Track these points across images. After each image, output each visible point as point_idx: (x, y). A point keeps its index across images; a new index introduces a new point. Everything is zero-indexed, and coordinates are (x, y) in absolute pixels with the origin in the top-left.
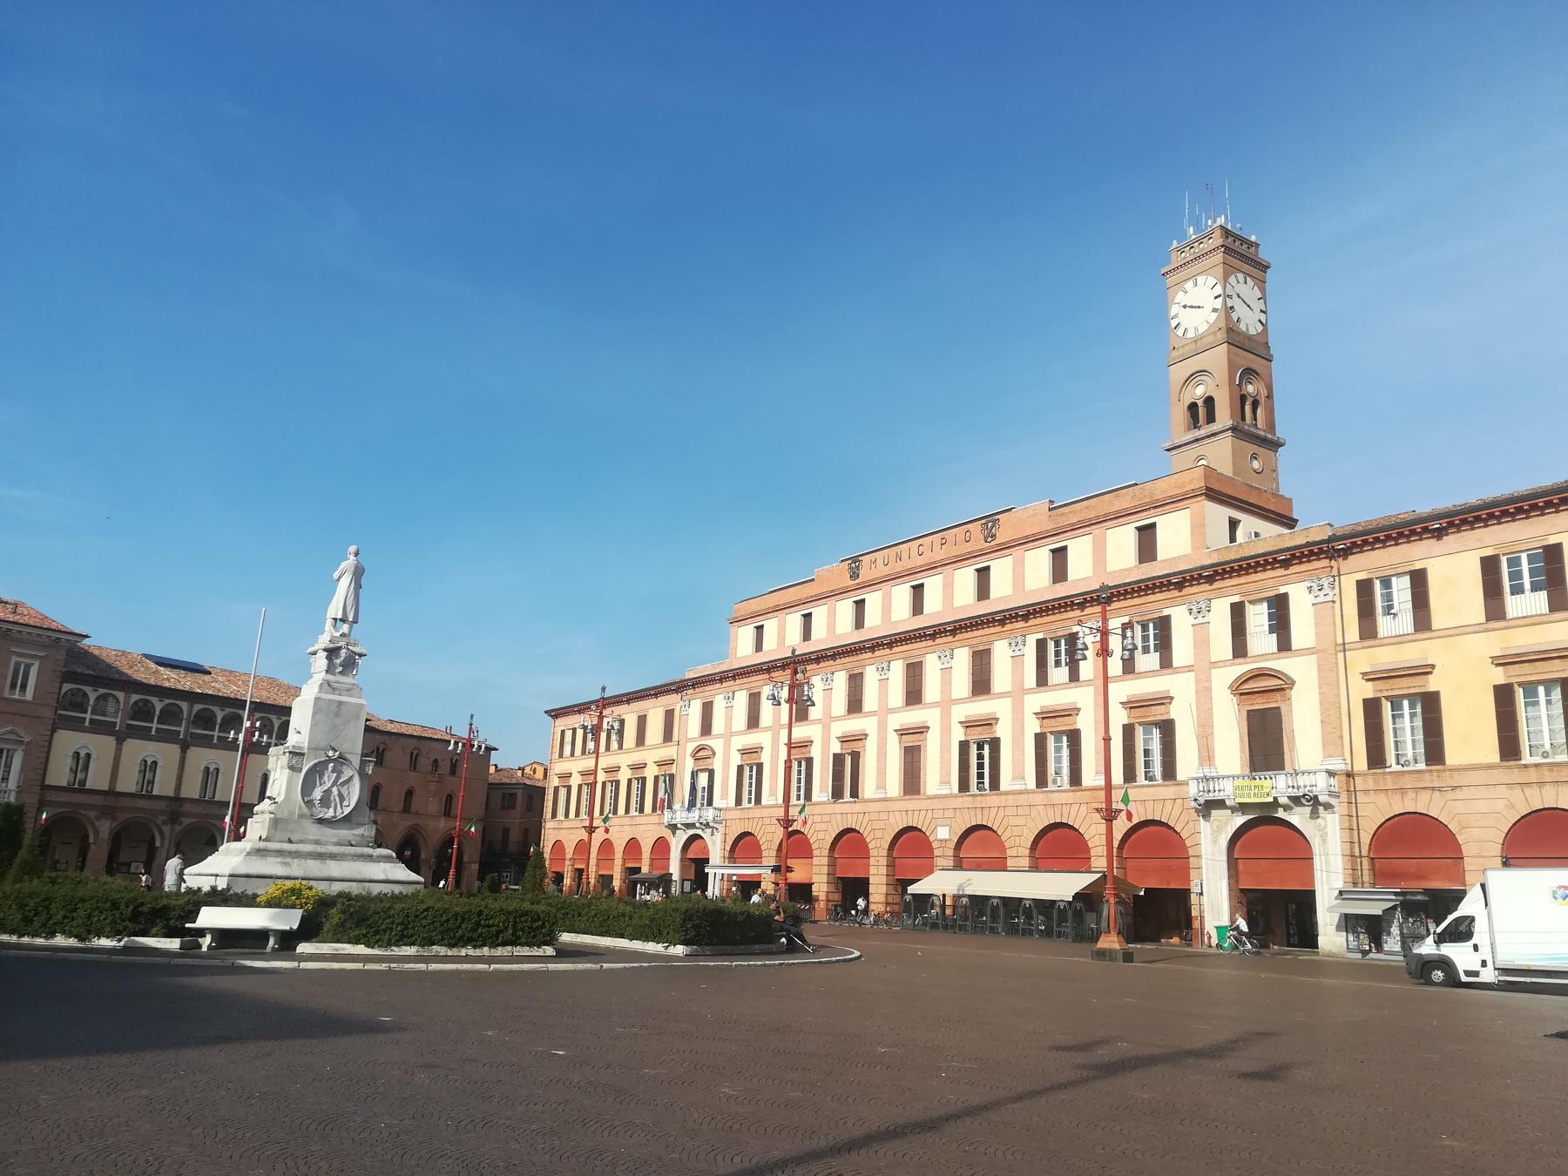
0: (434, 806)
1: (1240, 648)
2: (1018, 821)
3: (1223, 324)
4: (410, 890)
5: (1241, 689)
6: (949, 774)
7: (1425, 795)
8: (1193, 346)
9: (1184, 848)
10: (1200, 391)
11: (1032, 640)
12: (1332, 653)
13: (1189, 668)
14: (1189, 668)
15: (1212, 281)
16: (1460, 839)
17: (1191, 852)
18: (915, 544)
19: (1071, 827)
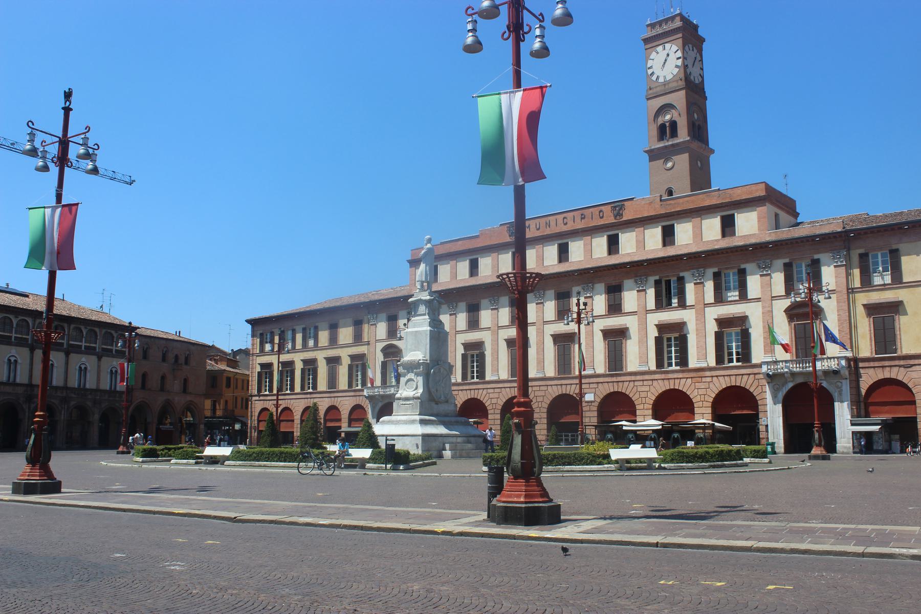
0: (177, 386)
2: (644, 389)
3: (682, 76)
4: (660, 427)
7: (895, 369)
8: (663, 88)
9: (756, 401)
10: (668, 117)
15: (675, 48)
17: (760, 402)
18: (560, 217)
19: (910, 390)
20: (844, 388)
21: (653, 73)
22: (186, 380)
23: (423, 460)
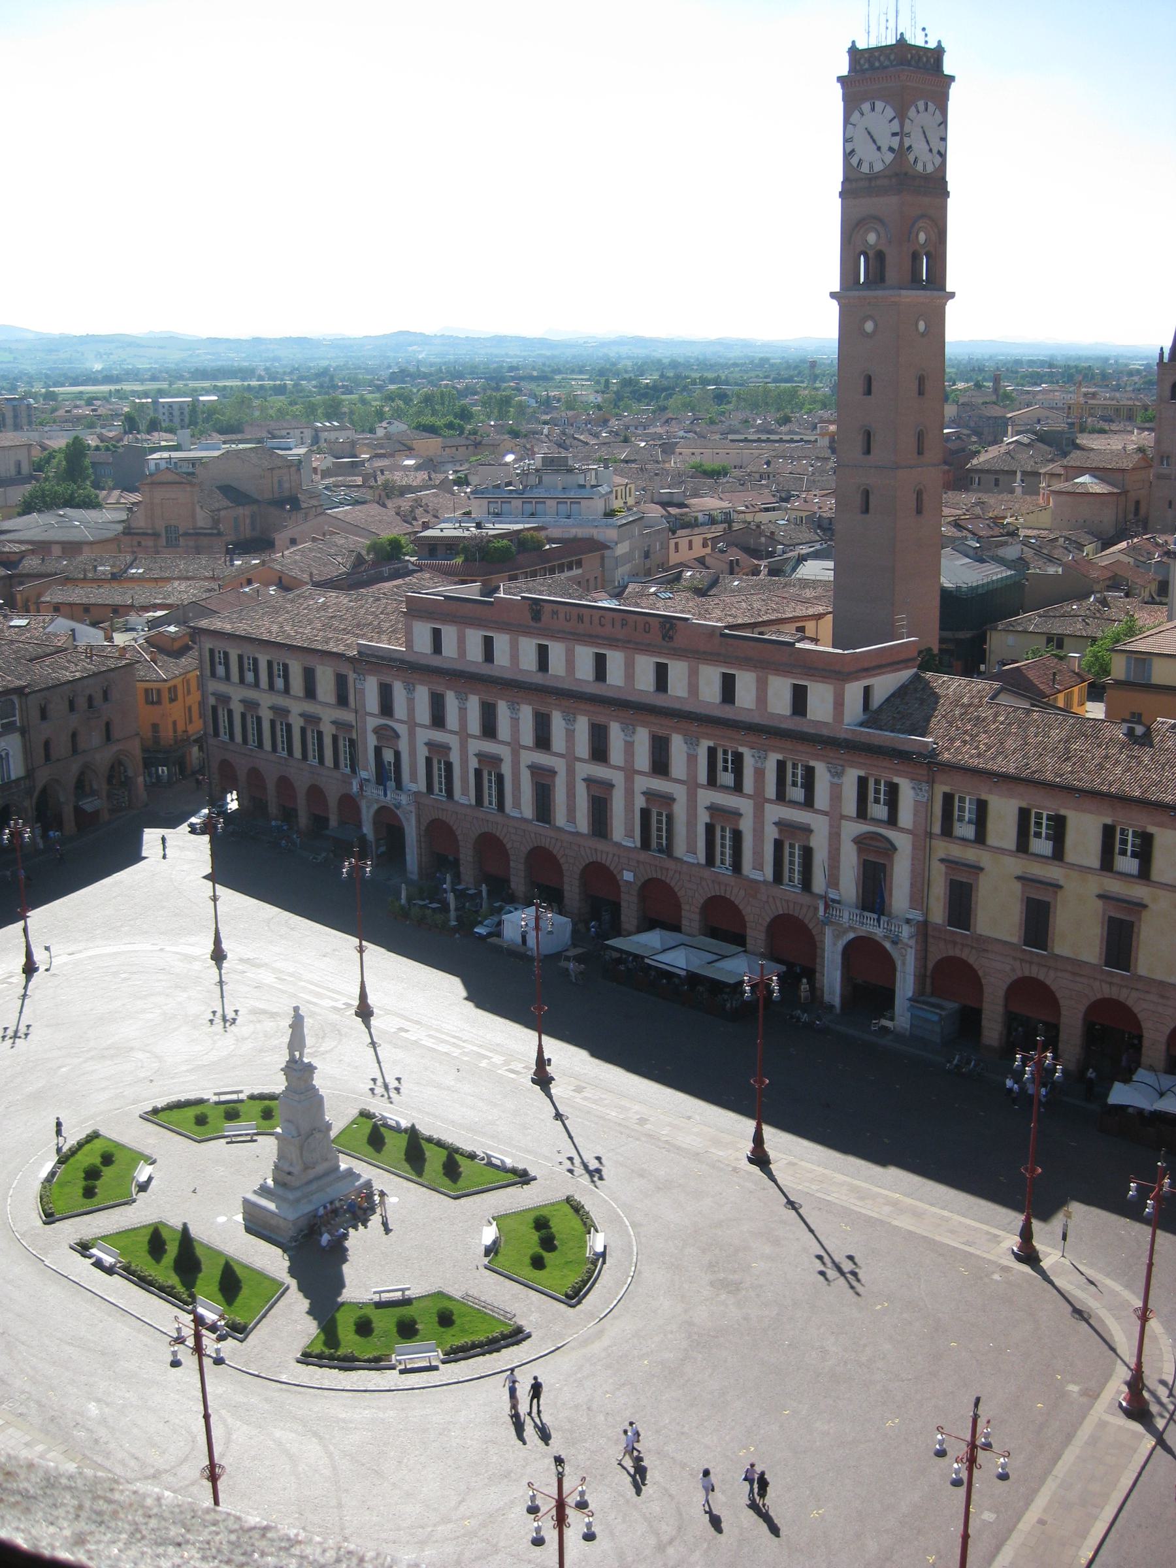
0: (96, 738)
1: (862, 813)
5: (861, 842)
6: (633, 830)
11: (705, 744)
12: (922, 838)
13: (508, 744)
14: (825, 813)
16: (983, 981)
20: (908, 957)
21: (860, 162)
22: (108, 725)
23: (142, 381)
